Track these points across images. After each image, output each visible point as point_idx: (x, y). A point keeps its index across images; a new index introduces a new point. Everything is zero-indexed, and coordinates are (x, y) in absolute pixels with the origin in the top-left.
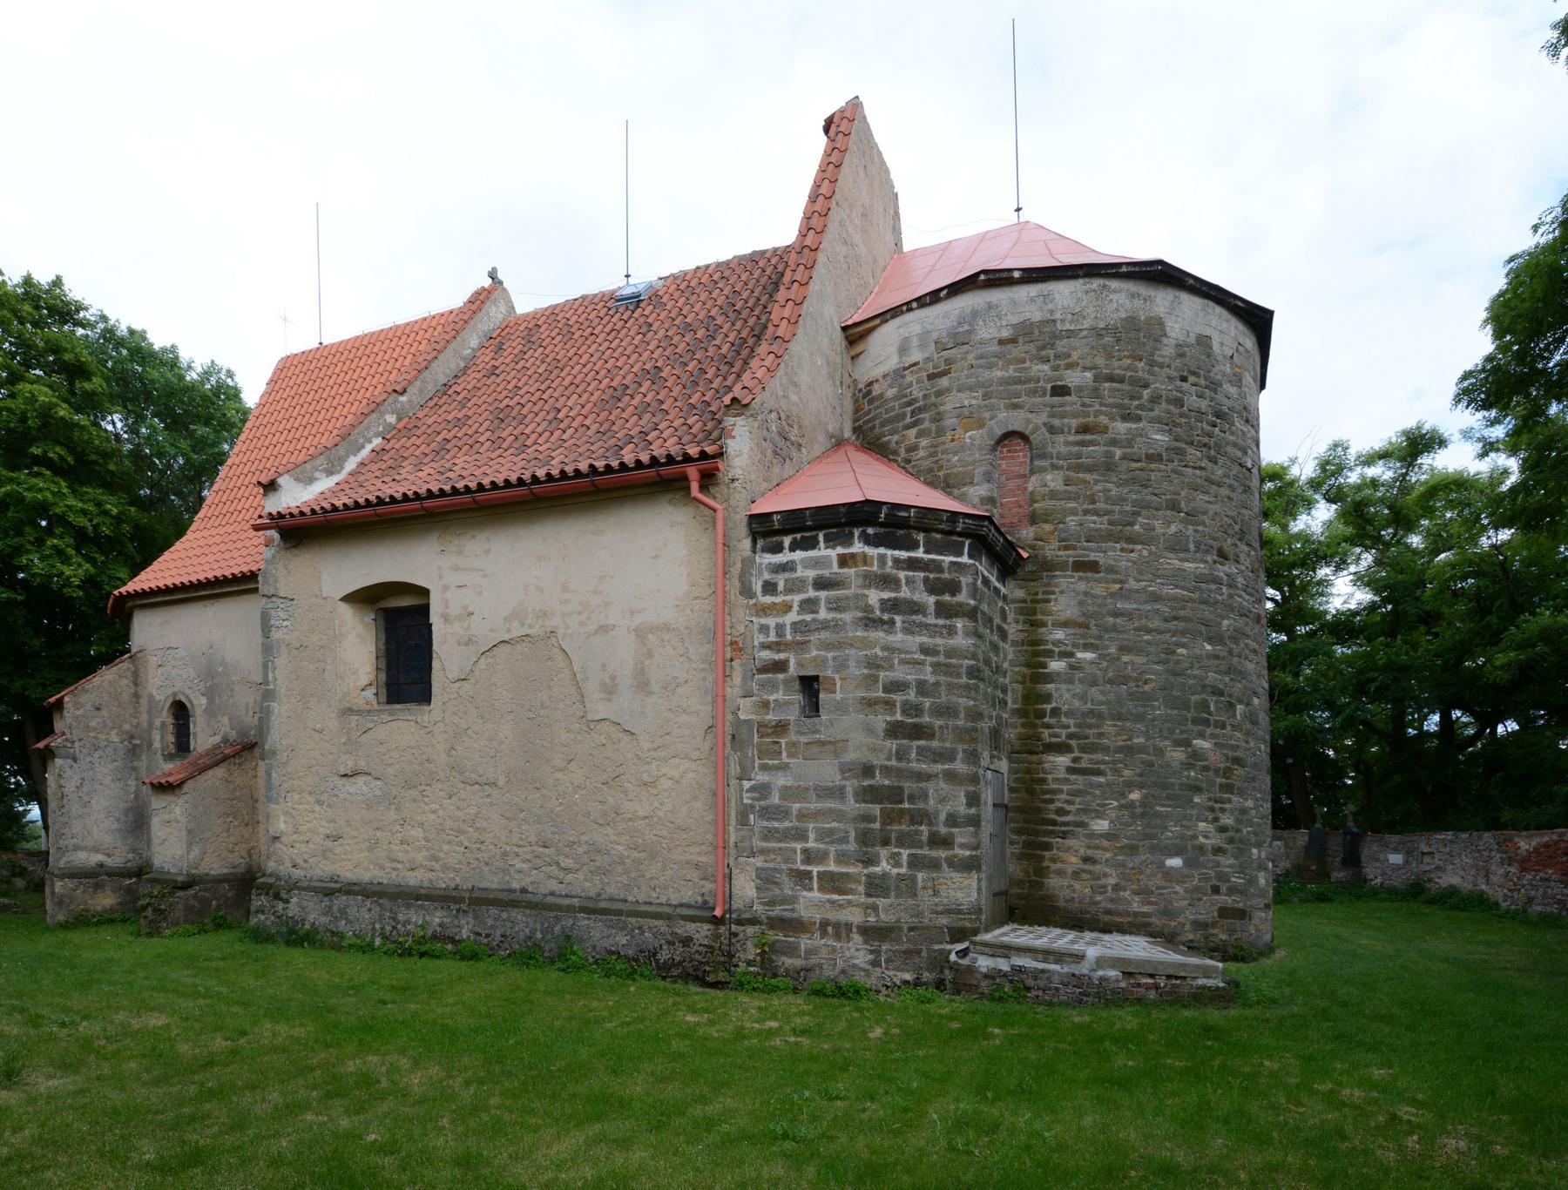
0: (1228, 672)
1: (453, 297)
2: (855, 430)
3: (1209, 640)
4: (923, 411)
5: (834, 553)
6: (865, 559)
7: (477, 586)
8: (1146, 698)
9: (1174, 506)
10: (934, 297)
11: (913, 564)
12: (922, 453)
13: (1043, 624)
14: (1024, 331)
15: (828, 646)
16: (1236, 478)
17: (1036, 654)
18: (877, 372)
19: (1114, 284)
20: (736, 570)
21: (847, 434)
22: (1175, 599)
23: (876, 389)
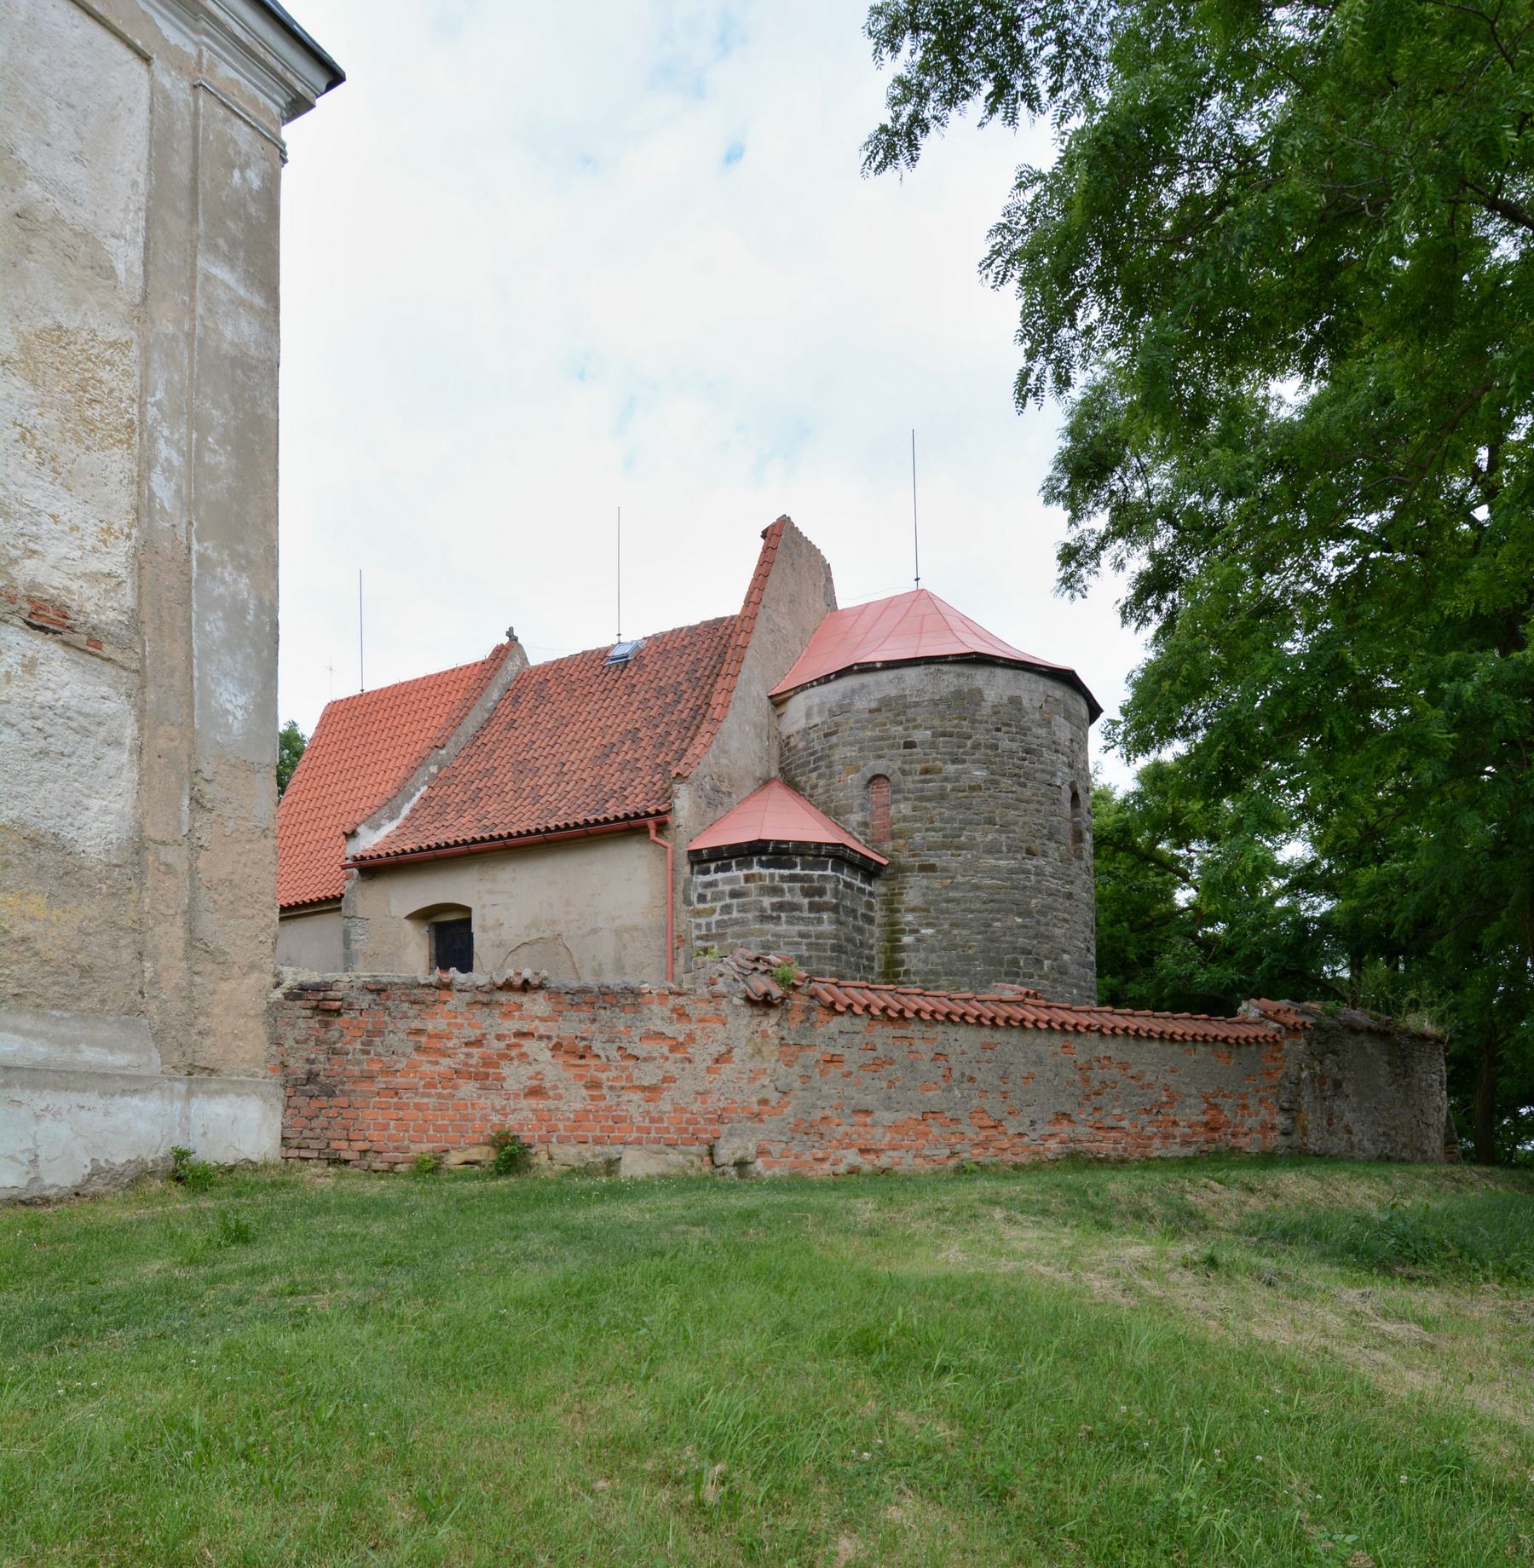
0: (1036, 937)
1: (480, 651)
2: (781, 770)
3: (1019, 915)
4: (820, 759)
5: (741, 874)
6: (761, 877)
7: (505, 905)
8: (969, 960)
9: (991, 821)
10: (826, 679)
11: (793, 878)
12: (820, 790)
13: (898, 911)
14: (885, 704)
15: (738, 936)
16: (1044, 795)
17: (894, 932)
18: (793, 729)
19: (945, 668)
20: (680, 887)
21: (774, 773)
22: (991, 887)
23: (793, 742)
